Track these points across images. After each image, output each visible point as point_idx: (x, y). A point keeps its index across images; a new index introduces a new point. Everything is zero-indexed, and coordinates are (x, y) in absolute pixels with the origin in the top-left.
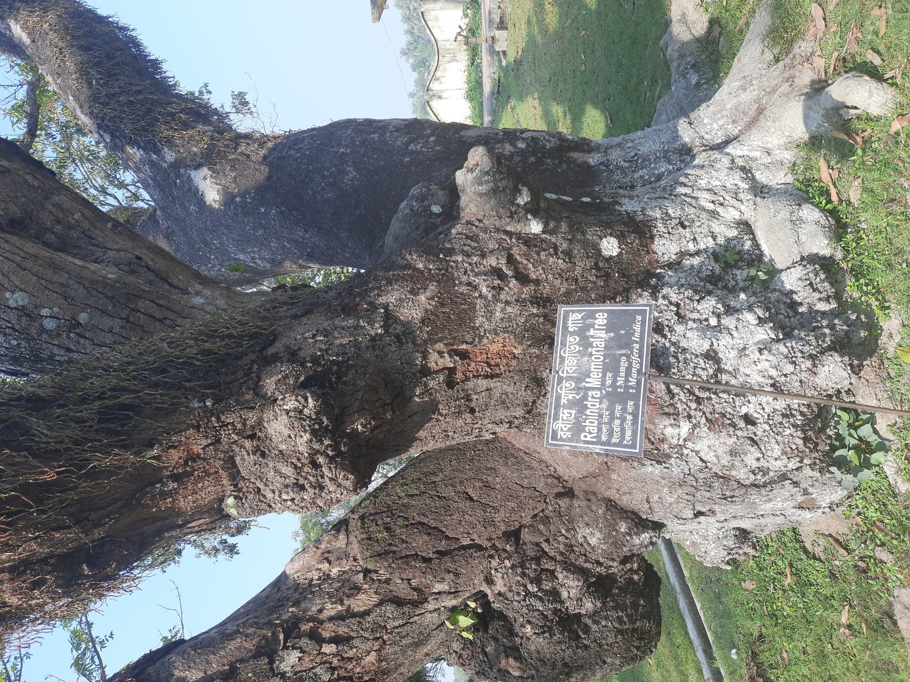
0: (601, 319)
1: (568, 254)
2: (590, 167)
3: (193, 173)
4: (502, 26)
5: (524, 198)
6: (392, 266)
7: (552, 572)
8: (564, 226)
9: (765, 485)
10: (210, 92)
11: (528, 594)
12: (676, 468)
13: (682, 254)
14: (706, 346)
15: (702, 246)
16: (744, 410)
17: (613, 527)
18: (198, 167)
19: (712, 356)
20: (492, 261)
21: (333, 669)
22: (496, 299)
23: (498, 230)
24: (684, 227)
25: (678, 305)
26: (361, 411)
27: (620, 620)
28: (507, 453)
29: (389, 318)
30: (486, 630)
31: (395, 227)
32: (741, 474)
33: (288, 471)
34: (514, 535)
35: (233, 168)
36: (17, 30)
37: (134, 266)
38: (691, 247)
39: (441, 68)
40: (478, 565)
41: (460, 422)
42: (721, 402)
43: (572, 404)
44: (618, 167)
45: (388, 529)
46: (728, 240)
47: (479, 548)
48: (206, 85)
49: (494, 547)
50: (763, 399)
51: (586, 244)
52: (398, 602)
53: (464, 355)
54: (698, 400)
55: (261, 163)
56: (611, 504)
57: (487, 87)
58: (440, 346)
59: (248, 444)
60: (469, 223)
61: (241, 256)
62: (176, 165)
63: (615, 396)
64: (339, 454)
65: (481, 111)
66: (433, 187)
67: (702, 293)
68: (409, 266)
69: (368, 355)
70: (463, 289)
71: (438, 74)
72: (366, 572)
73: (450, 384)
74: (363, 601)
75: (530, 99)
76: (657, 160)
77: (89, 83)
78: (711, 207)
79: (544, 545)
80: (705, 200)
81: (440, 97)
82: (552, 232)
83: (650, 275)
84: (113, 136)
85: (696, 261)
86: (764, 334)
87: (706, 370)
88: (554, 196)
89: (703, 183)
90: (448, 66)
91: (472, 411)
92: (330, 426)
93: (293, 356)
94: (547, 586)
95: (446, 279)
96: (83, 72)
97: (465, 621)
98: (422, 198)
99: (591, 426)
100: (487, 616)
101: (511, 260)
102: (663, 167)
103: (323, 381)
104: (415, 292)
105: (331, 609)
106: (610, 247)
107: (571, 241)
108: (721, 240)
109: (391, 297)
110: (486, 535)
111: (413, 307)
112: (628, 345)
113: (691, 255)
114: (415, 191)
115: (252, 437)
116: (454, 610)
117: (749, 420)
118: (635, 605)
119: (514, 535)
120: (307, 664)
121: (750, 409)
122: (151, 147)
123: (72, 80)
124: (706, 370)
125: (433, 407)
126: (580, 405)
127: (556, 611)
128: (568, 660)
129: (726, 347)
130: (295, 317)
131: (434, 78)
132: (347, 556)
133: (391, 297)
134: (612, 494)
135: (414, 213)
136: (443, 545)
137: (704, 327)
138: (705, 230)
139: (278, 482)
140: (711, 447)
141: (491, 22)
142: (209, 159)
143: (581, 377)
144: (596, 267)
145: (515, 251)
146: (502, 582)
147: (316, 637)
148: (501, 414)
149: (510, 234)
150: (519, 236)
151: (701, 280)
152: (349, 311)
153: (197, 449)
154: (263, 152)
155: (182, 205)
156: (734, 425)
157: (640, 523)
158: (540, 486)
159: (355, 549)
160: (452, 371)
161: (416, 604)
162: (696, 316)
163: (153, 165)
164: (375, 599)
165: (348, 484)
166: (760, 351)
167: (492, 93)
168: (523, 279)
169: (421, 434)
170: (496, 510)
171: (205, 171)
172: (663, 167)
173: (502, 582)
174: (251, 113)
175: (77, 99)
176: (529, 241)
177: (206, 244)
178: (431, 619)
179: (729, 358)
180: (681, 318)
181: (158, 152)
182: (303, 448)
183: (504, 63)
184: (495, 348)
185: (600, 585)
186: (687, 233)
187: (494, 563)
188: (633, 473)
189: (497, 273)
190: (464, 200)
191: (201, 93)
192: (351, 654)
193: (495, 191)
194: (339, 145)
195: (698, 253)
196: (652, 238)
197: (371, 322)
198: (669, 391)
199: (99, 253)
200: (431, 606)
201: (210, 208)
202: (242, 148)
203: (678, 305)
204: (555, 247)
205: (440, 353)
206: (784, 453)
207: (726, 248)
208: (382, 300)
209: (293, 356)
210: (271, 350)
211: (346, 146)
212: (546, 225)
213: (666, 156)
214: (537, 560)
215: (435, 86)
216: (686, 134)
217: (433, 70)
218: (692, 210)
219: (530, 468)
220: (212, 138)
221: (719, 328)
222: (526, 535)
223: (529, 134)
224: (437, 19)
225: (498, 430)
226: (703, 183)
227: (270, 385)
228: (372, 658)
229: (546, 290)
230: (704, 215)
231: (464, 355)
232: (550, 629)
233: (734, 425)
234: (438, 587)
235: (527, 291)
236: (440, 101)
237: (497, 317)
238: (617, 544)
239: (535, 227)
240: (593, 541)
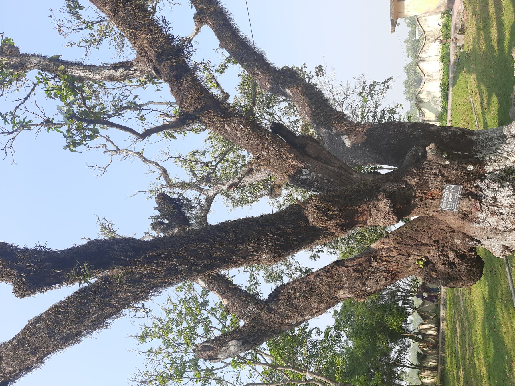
0: (453, 187)
1: (457, 170)
2: (472, 140)
3: (342, 137)
4: (462, 32)
5: (445, 155)
6: (408, 171)
7: (447, 251)
8: (456, 162)
9: (508, 232)
10: (306, 67)
11: (439, 255)
12: (482, 225)
13: (494, 170)
14: (493, 195)
15: (501, 168)
16: (501, 211)
17: (464, 240)
18: (344, 135)
19: (494, 198)
20: (435, 171)
21: (385, 268)
22: (435, 180)
23: (437, 163)
24: (496, 162)
25: (487, 184)
26: (399, 204)
27: (466, 266)
28: (437, 221)
29: (407, 184)
30: (427, 266)
31: (407, 158)
32: (500, 228)
33: (383, 214)
34: (437, 242)
35: (355, 136)
36: (288, 91)
37: (340, 168)
38: (497, 168)
39: (426, 46)
40: (426, 249)
41: (423, 210)
42: (495, 209)
43: (445, 202)
44: (482, 141)
45: (401, 238)
46: (510, 166)
47: (427, 244)
48: (304, 64)
49: (431, 244)
50: (506, 209)
51: (462, 167)
52: (403, 255)
53: (425, 194)
54: (489, 208)
55: (364, 135)
56: (464, 234)
57: (452, 59)
58: (419, 191)
59: (374, 208)
60: (429, 161)
61: (354, 161)
62: (336, 134)
63: (454, 201)
64: (394, 212)
65: (448, 70)
66: (420, 147)
67: (495, 181)
68: (412, 171)
69: (401, 192)
70: (426, 178)
71: (424, 49)
72: (394, 247)
73: (421, 200)
74: (394, 254)
75: (472, 74)
76: (495, 139)
77: (312, 110)
78: (507, 156)
79: (445, 244)
80: (505, 154)
81: (425, 61)
82: (453, 164)
83: (483, 175)
84: (317, 124)
85: (498, 172)
86: (510, 193)
87: (492, 201)
88: (456, 152)
89: (506, 149)
90: (431, 44)
91: (427, 207)
92: (393, 206)
93: (384, 191)
94: (445, 253)
95: (422, 175)
96: (310, 106)
97: (421, 263)
98: (416, 150)
99: (449, 206)
100: (428, 262)
101: (440, 171)
102: (497, 141)
103: (390, 196)
104: (413, 178)
105: (385, 255)
106: (470, 168)
107: (458, 166)
108: (508, 166)
109: (407, 179)
110: (429, 241)
111: (413, 182)
112: (457, 193)
113: (497, 170)
114: (414, 148)
115: (375, 207)
116: (418, 260)
117: (502, 214)
118: (472, 264)
119: (437, 242)
120: (379, 265)
121: (503, 211)
122: (329, 128)
123: (307, 108)
124: (492, 201)
125: (416, 205)
126: (447, 203)
127: (447, 260)
128: (450, 274)
129: (499, 196)
130: (384, 182)
131: (423, 51)
132: (389, 244)
133: (407, 179)
134: (465, 232)
135: (413, 155)
136: (416, 243)
137: (494, 190)
138: (503, 163)
139: (380, 217)
140: (492, 220)
141: (456, 29)
142: (348, 133)
143: (447, 198)
144: (465, 173)
145: (441, 169)
146: (432, 253)
147: (380, 259)
148: (435, 209)
149: (440, 164)
150: (443, 165)
151: (498, 177)
152: (397, 181)
153: (364, 208)
154: (364, 131)
155: (337, 145)
156: (497, 215)
157: (472, 239)
158: (445, 229)
159: (391, 242)
160: (422, 197)
161: (408, 257)
162: (492, 187)
163: (329, 133)
164: (397, 254)
165: (396, 219)
166: (507, 197)
167: (455, 63)
168: (443, 176)
169: (413, 212)
170: (432, 235)
171: (346, 136)
172: (497, 141)
173: (432, 253)
174: (323, 75)
175: (306, 113)
176: (445, 166)
177: (343, 157)
178: (412, 261)
179: (499, 198)
180: (488, 187)
181: (331, 130)
182: (387, 210)
183: (462, 50)
184: (434, 192)
185: (462, 257)
186: (497, 164)
187: (431, 248)
188: (470, 226)
189: (436, 174)
190: (428, 155)
191: (302, 68)
192: (390, 265)
193: (436, 154)
194: (390, 131)
195: (499, 170)
196: (485, 165)
197: (402, 185)
198: (481, 205)
199: (333, 164)
200: (412, 258)
201: (347, 147)
202: (357, 129)
203: (487, 184)
204: (453, 168)
205: (419, 193)
206: (511, 222)
207: (509, 169)
208: (405, 179)
209: (384, 191)
210: (380, 190)
211: (392, 131)
212: (451, 162)
213: (498, 138)
214: (443, 247)
215: (422, 55)
216: (506, 132)
217: (422, 47)
218: (500, 157)
219: (442, 224)
220: (348, 126)
221: (498, 191)
222: (440, 242)
223: (452, 129)
224: (426, 20)
225: (434, 213)
226: (506, 149)
227: (380, 197)
228: (395, 267)
229: (449, 179)
230: (504, 159)
231: (425, 194)
232: (445, 264)
233: (497, 215)
234: (414, 253)
235: (444, 179)
236: (424, 63)
237: (434, 184)
238: (465, 244)
239: (448, 163)
240: (459, 243)
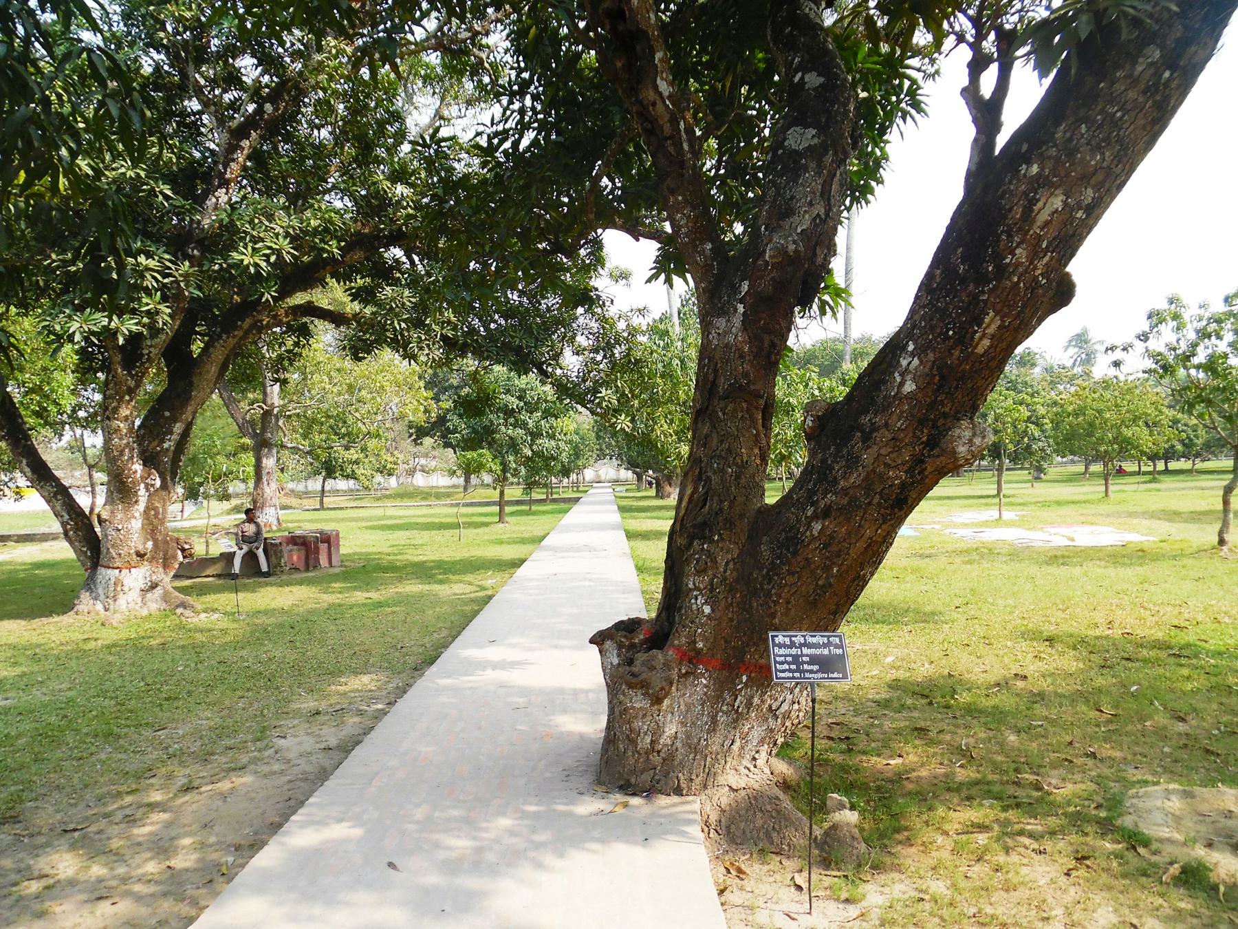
99: (782, 651)
